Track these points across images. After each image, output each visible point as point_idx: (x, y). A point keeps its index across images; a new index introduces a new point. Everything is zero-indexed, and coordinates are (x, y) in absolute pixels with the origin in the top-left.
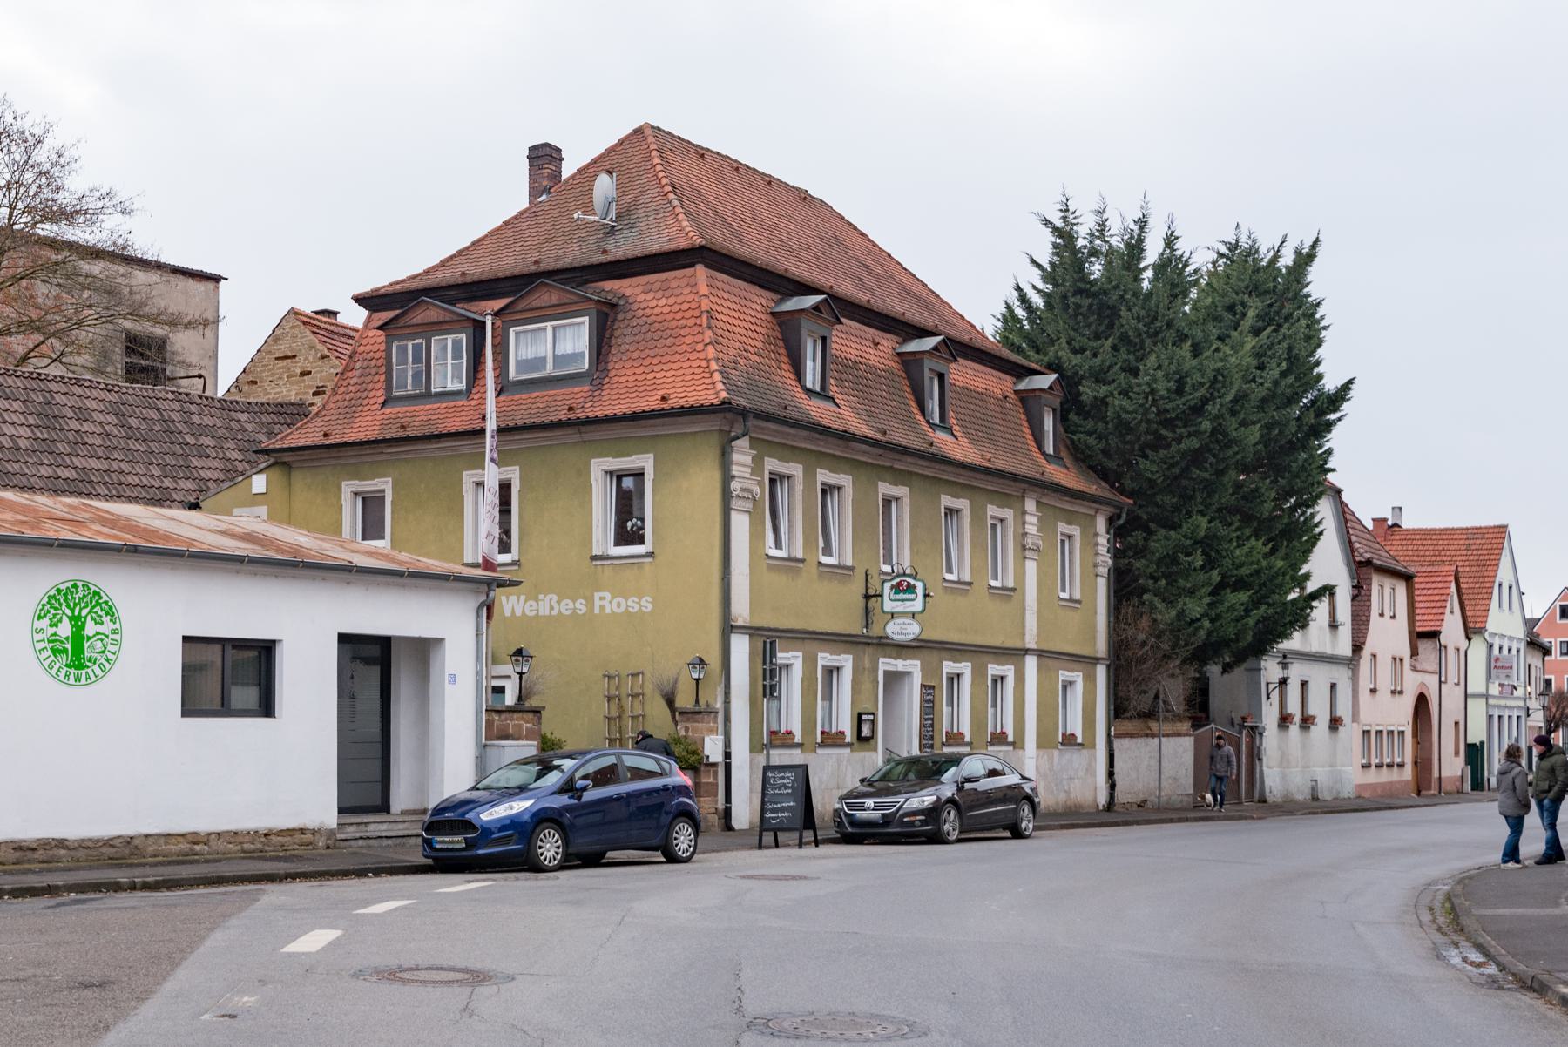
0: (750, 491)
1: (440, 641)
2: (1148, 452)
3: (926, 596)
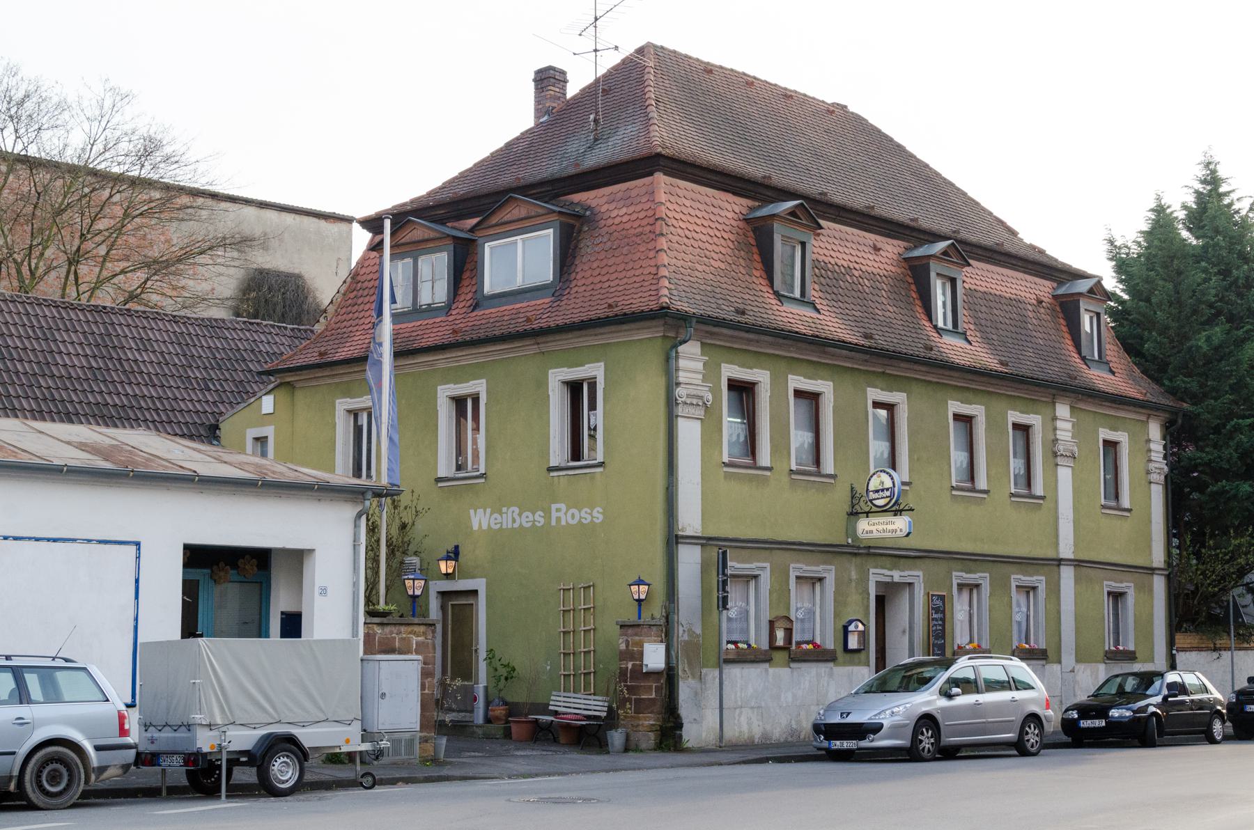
1: (311, 551)
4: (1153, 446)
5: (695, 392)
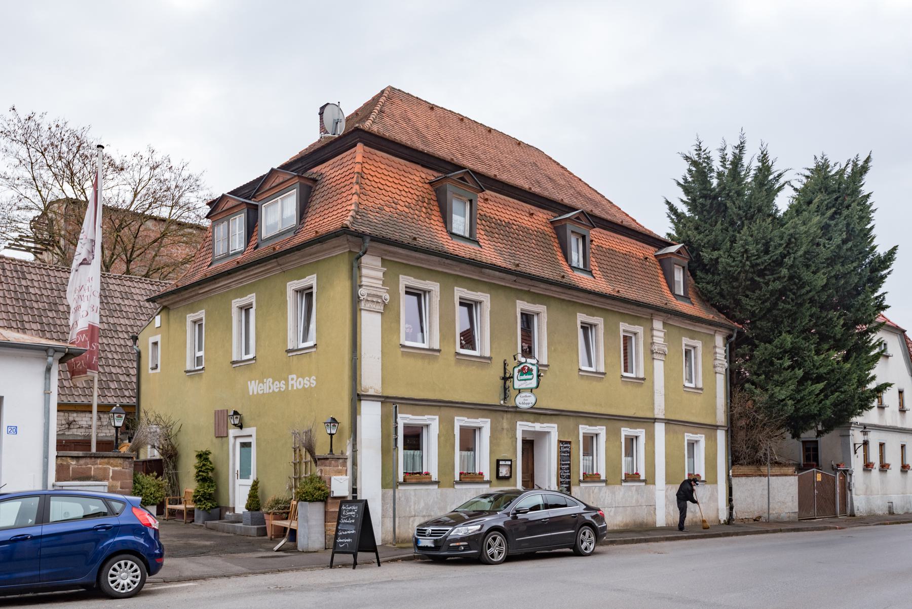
0: (380, 297)
2: (748, 293)
3: (539, 376)
4: (718, 350)
5: (375, 293)
